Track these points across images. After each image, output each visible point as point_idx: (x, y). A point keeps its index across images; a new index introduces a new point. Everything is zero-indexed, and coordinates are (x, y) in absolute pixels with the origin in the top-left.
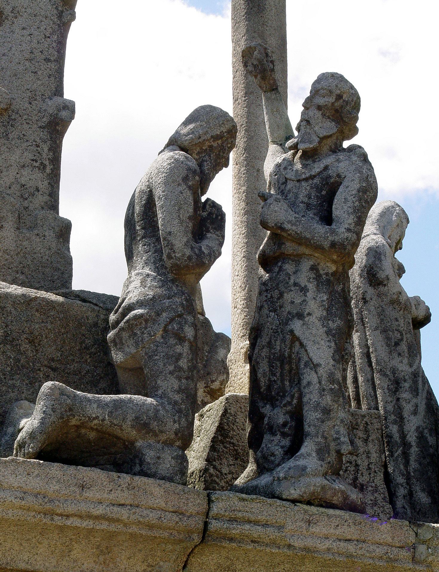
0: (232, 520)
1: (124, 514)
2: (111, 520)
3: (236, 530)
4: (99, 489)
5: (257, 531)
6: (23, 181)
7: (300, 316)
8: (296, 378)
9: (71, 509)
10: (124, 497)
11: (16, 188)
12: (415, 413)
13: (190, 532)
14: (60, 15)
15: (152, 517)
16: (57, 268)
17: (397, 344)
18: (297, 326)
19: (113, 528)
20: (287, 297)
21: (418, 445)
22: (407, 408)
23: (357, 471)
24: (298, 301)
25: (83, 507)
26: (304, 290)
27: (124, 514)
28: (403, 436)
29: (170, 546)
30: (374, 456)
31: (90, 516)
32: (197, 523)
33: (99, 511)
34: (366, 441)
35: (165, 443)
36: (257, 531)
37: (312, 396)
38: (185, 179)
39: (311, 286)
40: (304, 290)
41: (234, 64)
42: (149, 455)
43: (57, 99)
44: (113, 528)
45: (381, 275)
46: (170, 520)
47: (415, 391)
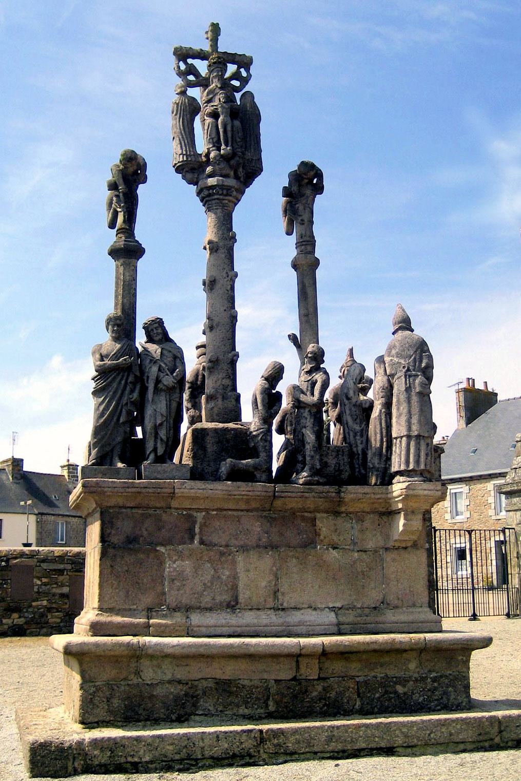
0: (282, 492)
1: (250, 493)
2: (247, 495)
3: (283, 494)
4: (243, 488)
5: (289, 494)
6: (223, 383)
7: (305, 427)
8: (304, 446)
9: (236, 493)
10: (251, 489)
11: (221, 386)
12: (361, 443)
13: (269, 497)
14: (232, 322)
15: (259, 493)
16: (236, 415)
17: (356, 420)
18: (304, 430)
19: (248, 497)
20: (302, 421)
21: (362, 454)
22: (359, 442)
23: (339, 465)
24: (304, 422)
25: (239, 493)
26: (306, 419)
27: (250, 493)
28: (358, 452)
29: (51, 621)
30: (346, 460)
31: (241, 495)
32: (271, 494)
33: (244, 493)
34: (343, 455)
35: (263, 472)
36: (289, 494)
37: (308, 453)
38: (265, 391)
39: (309, 417)
40: (306, 419)
41: (270, 364)
42: (258, 476)
43: (233, 352)
44: (248, 497)
45: (349, 396)
46: (263, 494)
47: (362, 436)
